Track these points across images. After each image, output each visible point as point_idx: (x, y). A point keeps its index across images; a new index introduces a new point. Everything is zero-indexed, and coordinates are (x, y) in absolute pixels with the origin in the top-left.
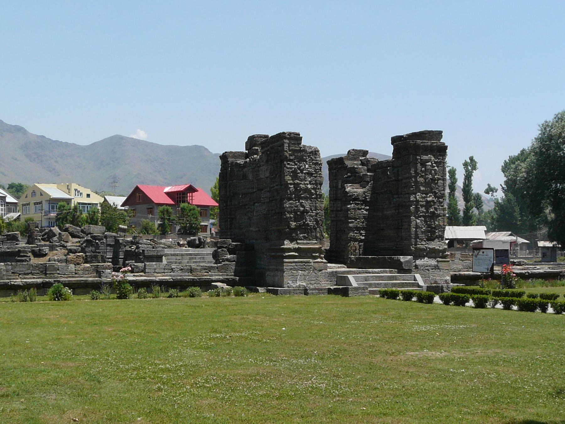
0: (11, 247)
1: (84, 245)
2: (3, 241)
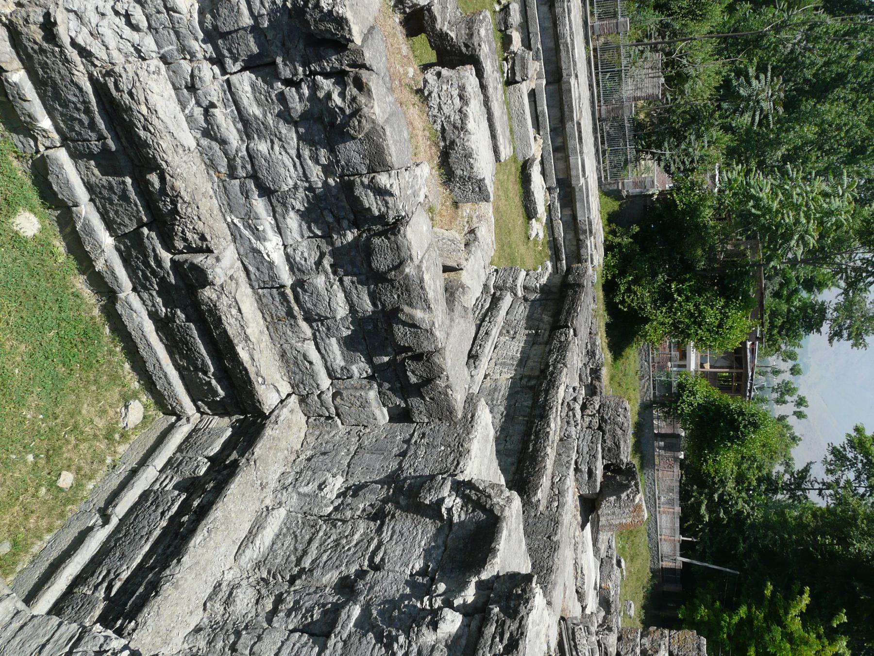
0: (568, 449)
1: (452, 502)
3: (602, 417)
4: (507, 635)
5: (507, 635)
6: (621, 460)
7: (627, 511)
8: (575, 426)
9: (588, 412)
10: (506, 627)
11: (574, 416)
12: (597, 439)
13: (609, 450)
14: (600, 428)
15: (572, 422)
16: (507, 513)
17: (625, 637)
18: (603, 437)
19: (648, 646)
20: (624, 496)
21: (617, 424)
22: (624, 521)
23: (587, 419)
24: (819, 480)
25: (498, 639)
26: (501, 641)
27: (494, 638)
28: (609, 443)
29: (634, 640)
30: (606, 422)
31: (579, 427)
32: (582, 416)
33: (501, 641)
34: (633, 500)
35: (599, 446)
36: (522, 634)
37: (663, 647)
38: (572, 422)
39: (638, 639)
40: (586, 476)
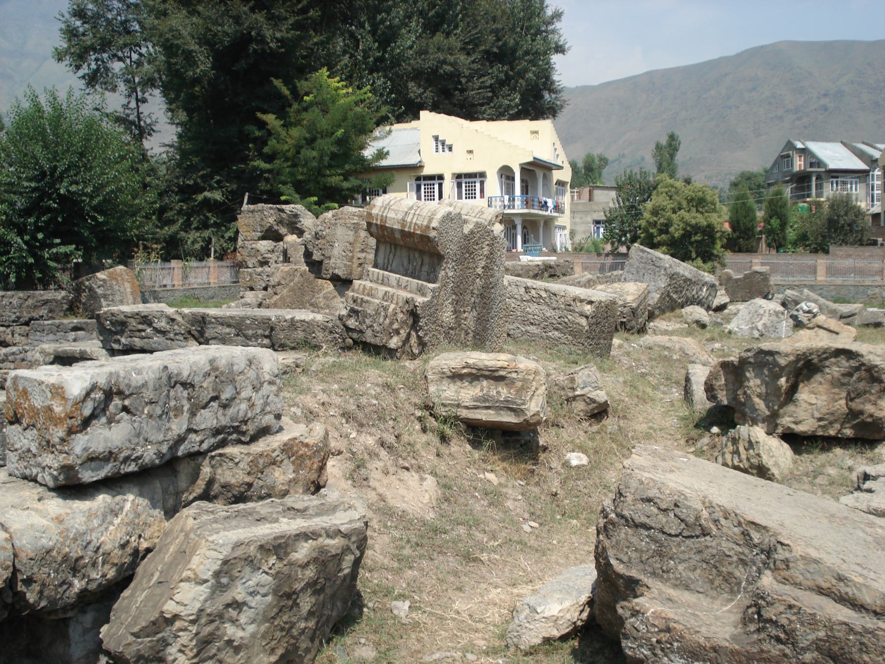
2: (31, 319)
3: (14, 321)
4: (140, 327)
5: (140, 327)
6: (63, 298)
7: (116, 288)
8: (26, 352)
9: (9, 338)
10: (134, 329)
11: (13, 354)
12: (40, 325)
13: (51, 311)
14: (27, 324)
15: (22, 356)
16: (51, 351)
17: (249, 284)
18: (37, 319)
19: (254, 260)
20: (100, 291)
21: (21, 304)
22: (129, 290)
23: (17, 339)
24: (125, 101)
25: (143, 334)
26: (144, 331)
27: (142, 338)
28: (43, 312)
29: (251, 274)
30: (19, 318)
31: (27, 348)
32: (15, 345)
33: (144, 331)
34: (104, 280)
35: (46, 322)
36: (137, 314)
37: (254, 246)
38: (22, 356)
39: (250, 270)
40: (80, 333)
